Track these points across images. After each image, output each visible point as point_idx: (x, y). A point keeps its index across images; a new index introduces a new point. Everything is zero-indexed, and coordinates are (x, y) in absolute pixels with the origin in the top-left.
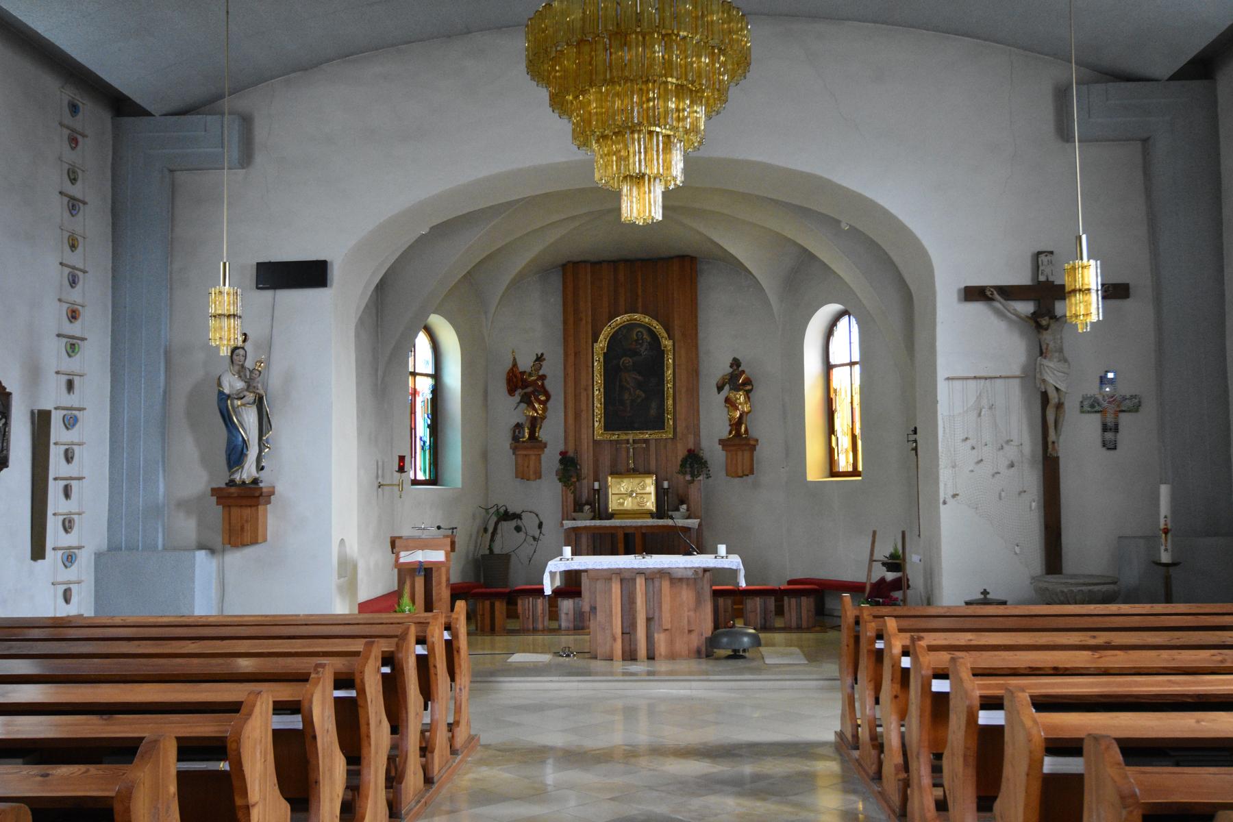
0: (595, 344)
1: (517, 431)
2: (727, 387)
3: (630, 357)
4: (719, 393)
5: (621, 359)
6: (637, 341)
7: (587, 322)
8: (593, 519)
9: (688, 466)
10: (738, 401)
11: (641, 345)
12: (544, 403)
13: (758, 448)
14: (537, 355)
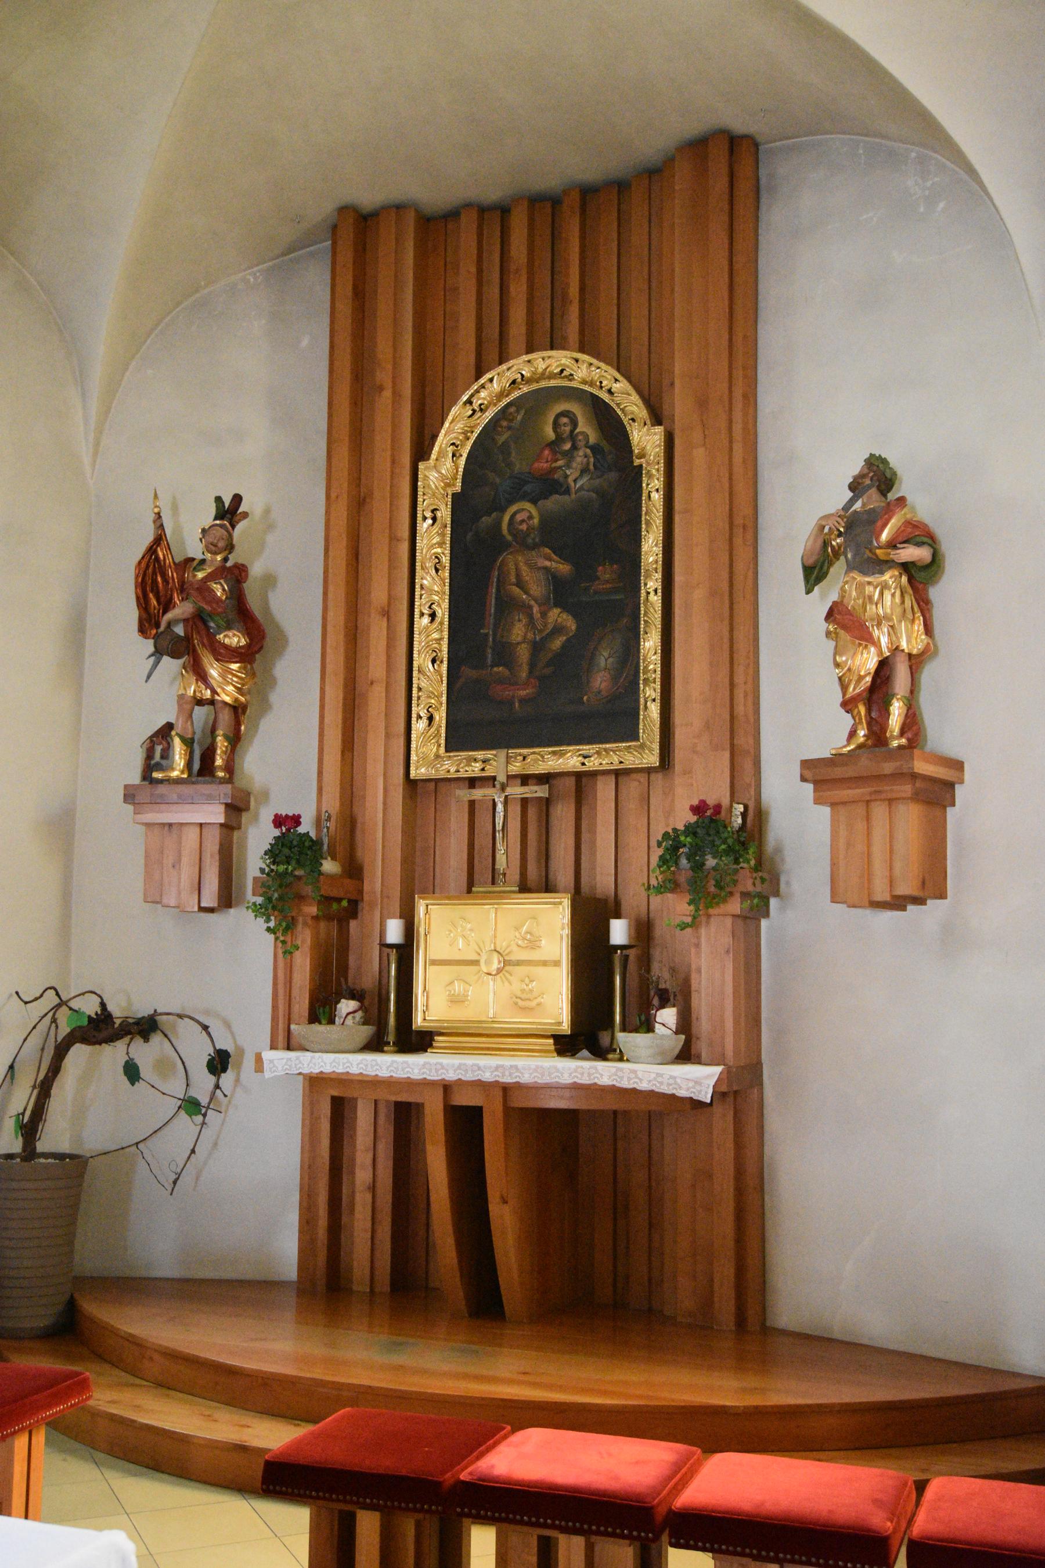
0: (421, 466)
1: (158, 749)
2: (838, 568)
3: (534, 502)
4: (808, 591)
5: (503, 510)
6: (553, 445)
7: (396, 394)
8: (375, 1045)
9: (684, 862)
10: (871, 609)
11: (569, 455)
12: (245, 656)
13: (959, 791)
14: (219, 500)
